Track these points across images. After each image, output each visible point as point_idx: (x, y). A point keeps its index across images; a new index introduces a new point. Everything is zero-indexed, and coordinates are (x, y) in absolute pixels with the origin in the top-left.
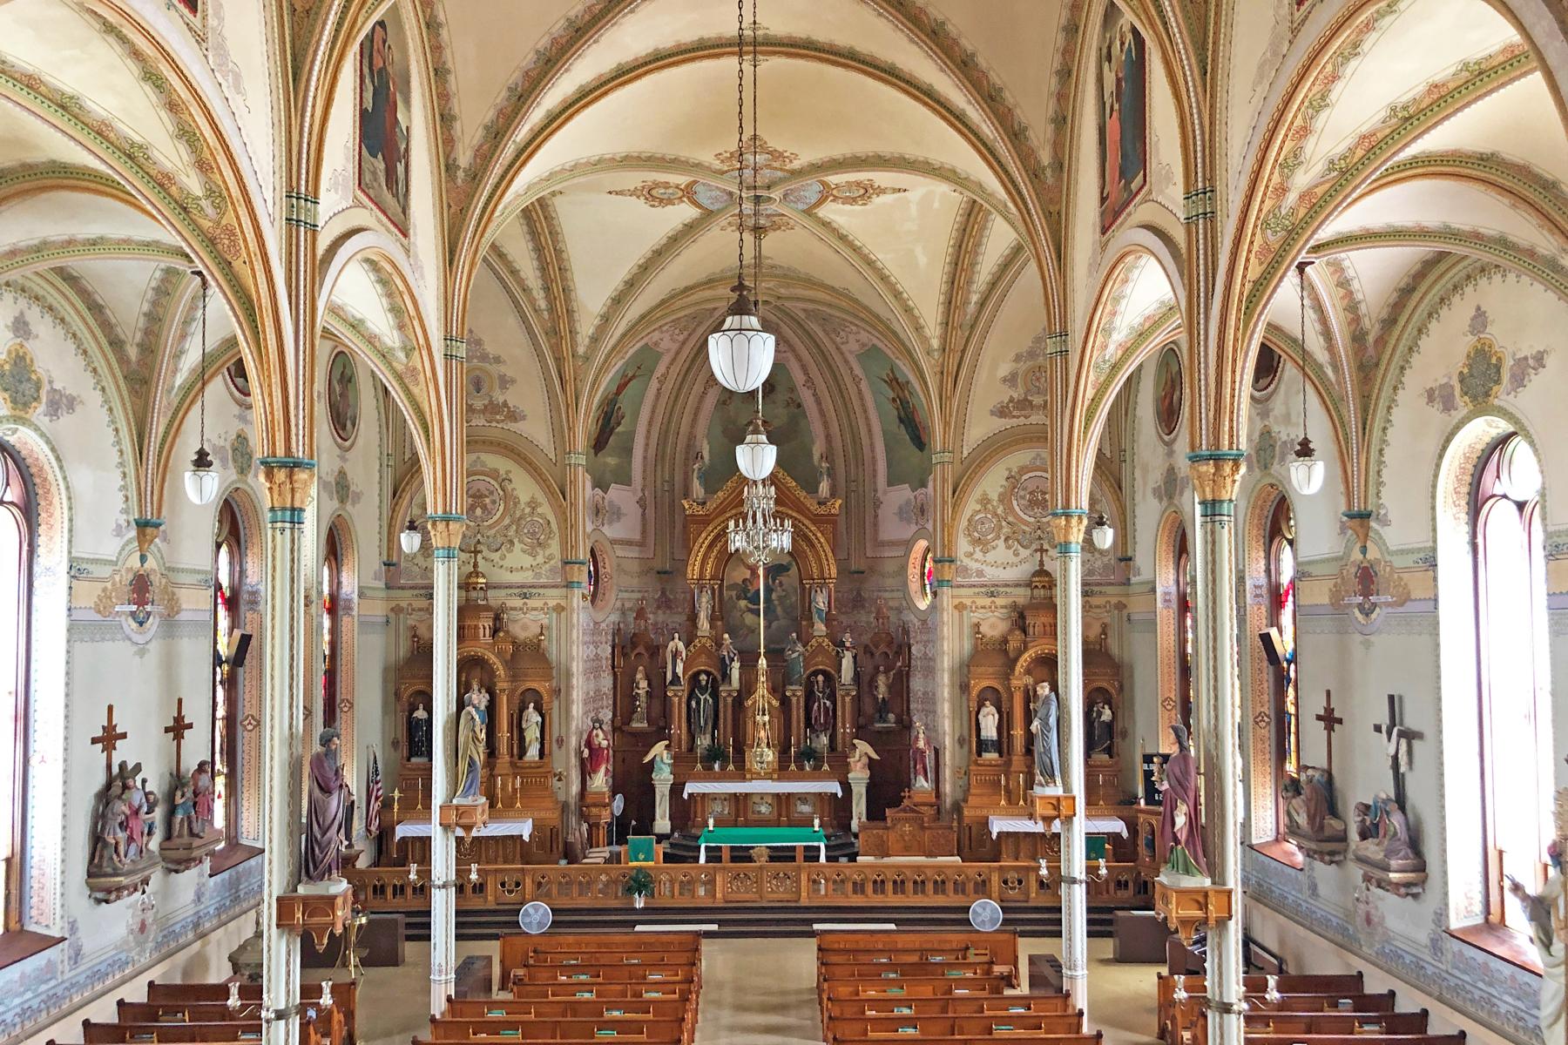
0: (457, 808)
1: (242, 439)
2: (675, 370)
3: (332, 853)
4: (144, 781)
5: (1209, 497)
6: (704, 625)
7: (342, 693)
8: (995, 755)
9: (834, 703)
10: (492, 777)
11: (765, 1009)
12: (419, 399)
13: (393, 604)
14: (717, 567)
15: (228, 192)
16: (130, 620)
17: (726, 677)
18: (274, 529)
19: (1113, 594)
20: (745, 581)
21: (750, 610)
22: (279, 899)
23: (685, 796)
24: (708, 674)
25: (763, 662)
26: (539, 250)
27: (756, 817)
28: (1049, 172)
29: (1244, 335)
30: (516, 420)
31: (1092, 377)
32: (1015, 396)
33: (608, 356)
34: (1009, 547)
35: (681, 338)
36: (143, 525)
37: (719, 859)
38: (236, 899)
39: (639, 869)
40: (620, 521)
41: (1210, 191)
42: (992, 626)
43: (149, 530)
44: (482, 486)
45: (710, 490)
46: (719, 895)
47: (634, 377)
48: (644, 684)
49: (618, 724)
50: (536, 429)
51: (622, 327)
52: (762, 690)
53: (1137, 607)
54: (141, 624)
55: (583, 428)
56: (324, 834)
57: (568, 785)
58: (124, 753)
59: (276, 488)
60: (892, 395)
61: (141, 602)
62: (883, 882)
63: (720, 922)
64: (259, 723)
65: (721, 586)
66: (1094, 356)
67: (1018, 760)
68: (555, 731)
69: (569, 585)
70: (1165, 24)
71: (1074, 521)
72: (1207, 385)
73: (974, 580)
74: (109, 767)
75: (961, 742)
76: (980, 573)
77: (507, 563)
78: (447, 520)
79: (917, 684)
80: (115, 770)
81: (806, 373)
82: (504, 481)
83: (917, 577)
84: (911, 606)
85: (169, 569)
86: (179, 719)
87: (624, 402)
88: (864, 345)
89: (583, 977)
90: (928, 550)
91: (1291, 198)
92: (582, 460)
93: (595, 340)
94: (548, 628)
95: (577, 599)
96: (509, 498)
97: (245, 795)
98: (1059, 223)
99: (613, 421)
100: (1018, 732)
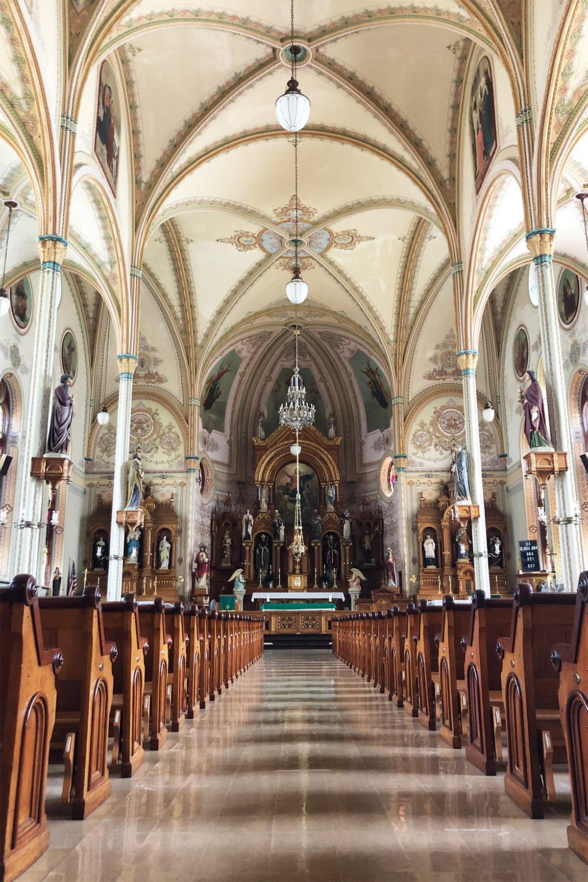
2: (249, 372)
5: (538, 254)
6: (264, 506)
8: (434, 567)
9: (339, 552)
10: (140, 578)
12: (116, 293)
13: (88, 482)
14: (272, 477)
15: (35, 94)
17: (277, 535)
19: (498, 476)
21: (290, 501)
22: (33, 459)
23: (253, 600)
24: (266, 534)
25: (298, 496)
26: (179, 281)
28: (447, 183)
29: (551, 168)
30: (162, 382)
31: (476, 278)
32: (437, 368)
33: (213, 349)
34: (437, 450)
35: (253, 350)
40: (218, 451)
41: (528, 110)
42: (430, 494)
44: (141, 417)
46: (273, 629)
47: (227, 371)
48: (229, 541)
49: (213, 565)
50: (173, 386)
51: (220, 333)
52: (298, 538)
53: (511, 482)
55: (199, 389)
60: (368, 380)
64: (12, 509)
65: (274, 486)
66: (477, 266)
67: (447, 569)
69: (188, 471)
70: (501, 39)
71: (471, 356)
72: (532, 190)
73: (418, 468)
75: (414, 561)
76: (421, 464)
77: (154, 459)
79: (387, 541)
81: (321, 373)
82: (154, 415)
83: (386, 481)
84: (383, 496)
88: (352, 352)
90: (392, 464)
91: (569, 94)
93: (207, 336)
94: (176, 495)
96: (157, 424)
98: (454, 208)
100: (447, 552)
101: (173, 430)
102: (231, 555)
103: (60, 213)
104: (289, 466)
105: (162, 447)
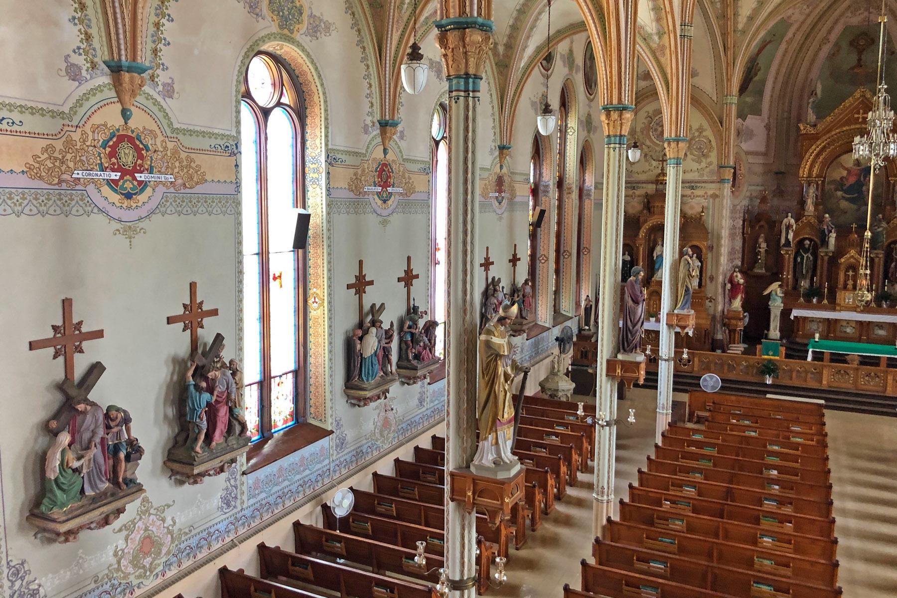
0: (677, 315)
1: (545, 96)
2: (799, 37)
3: (637, 338)
4: (503, 288)
6: (810, 207)
7: (584, 244)
11: (871, 459)
14: (821, 170)
16: (376, 197)
17: (825, 242)
18: (609, 148)
20: (842, 178)
22: (608, 361)
27: (843, 335)
35: (807, 11)
36: (502, 148)
37: (822, 360)
38: (537, 353)
39: (770, 361)
43: (505, 151)
45: (820, 117)
46: (824, 382)
47: (770, 42)
48: (764, 245)
54: (385, 201)
56: (634, 326)
57: (715, 306)
58: (494, 272)
59: (611, 124)
61: (500, 191)
62: (586, 352)
63: (826, 399)
64: (548, 259)
65: (823, 182)
68: (709, 272)
69: (722, 181)
74: (487, 279)
78: (677, 141)
80: (490, 280)
85: (512, 173)
86: (515, 255)
87: (761, 61)
89: (747, 422)
92: (735, 100)
93: (751, 19)
94: (707, 208)
95: (727, 188)
97: (540, 298)
99: (753, 73)
101: (704, 134)
102: (766, 260)
103: (625, 79)
104: (844, 157)
105: (692, 154)
